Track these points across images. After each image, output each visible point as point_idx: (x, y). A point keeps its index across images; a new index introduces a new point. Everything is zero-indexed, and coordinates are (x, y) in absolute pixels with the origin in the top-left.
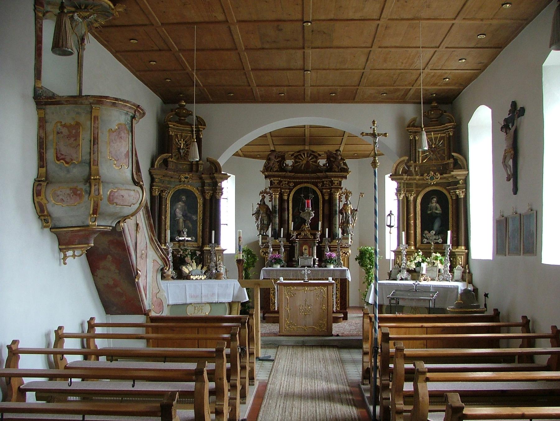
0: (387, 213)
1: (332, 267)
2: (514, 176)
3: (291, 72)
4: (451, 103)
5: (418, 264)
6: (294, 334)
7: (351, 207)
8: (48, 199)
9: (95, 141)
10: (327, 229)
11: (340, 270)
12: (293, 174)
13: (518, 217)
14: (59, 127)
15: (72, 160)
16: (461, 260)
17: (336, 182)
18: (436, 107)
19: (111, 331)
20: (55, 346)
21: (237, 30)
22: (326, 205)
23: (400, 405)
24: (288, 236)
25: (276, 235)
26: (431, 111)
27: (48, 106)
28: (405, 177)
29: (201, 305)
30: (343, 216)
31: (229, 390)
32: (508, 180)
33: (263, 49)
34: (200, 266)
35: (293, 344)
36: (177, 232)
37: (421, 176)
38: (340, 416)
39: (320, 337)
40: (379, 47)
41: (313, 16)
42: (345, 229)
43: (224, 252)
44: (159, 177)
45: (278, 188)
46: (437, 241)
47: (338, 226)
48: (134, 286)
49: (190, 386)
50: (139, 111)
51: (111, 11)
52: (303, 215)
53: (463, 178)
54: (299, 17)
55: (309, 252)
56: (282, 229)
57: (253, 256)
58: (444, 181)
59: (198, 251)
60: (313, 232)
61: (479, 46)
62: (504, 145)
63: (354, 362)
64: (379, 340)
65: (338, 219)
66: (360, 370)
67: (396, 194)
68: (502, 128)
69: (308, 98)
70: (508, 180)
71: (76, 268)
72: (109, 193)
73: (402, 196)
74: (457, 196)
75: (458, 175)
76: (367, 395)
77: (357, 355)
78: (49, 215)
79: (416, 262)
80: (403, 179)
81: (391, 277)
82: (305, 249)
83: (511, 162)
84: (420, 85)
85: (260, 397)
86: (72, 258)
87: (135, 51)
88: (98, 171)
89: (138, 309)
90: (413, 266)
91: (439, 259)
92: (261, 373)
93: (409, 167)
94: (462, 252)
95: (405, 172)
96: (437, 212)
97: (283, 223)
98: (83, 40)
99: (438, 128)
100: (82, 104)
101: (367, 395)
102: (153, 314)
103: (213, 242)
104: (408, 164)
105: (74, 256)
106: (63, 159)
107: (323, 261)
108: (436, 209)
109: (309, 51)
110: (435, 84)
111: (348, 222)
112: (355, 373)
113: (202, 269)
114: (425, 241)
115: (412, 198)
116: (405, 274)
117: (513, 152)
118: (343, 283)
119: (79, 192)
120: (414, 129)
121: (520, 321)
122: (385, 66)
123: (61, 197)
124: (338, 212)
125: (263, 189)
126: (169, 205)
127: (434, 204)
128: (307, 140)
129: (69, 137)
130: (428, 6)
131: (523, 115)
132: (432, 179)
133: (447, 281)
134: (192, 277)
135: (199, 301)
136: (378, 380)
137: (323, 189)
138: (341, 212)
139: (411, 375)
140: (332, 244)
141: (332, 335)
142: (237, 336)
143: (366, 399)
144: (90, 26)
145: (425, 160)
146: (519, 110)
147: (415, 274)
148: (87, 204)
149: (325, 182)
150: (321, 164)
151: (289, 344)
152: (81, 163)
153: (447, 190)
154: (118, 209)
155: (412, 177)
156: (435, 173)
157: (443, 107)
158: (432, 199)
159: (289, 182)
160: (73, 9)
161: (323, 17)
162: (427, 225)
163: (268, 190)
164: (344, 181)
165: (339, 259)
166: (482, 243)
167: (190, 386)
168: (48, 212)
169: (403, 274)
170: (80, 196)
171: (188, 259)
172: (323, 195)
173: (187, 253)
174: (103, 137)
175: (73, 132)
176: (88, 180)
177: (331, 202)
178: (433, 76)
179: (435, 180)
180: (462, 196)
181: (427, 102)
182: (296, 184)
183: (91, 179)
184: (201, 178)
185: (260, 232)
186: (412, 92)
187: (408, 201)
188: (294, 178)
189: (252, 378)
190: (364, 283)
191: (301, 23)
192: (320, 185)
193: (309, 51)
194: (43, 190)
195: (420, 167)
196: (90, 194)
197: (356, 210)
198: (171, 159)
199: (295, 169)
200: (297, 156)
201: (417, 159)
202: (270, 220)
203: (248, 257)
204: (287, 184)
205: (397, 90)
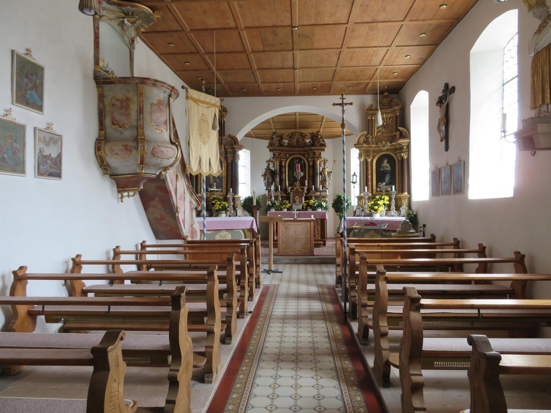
0: (352, 173)
2: (446, 138)
3: (285, 70)
4: (398, 93)
7: (327, 170)
8: (106, 152)
9: (141, 111)
13: (449, 168)
14: (114, 101)
15: (124, 125)
16: (405, 202)
18: (387, 96)
19: (159, 249)
20: (114, 259)
21: (244, 34)
23: (365, 300)
25: (276, 190)
26: (384, 98)
27: (105, 85)
31: (238, 291)
32: (442, 141)
33: (264, 51)
39: (307, 257)
40: (347, 48)
41: (299, 22)
48: (175, 219)
49: (202, 287)
50: (174, 92)
51: (151, 17)
53: (407, 144)
54: (288, 23)
58: (392, 147)
60: (302, 187)
61: (420, 44)
63: (330, 273)
64: (348, 253)
65: (319, 178)
66: (334, 277)
67: (359, 158)
68: (437, 103)
69: (297, 91)
70: (442, 141)
71: (132, 204)
72: (151, 149)
74: (402, 158)
75: (403, 143)
76: (340, 295)
77: (332, 268)
78: (108, 165)
80: (363, 147)
81: (355, 214)
83: (443, 128)
84: (376, 79)
85: (263, 296)
86: (127, 198)
87: (174, 54)
89: (178, 235)
92: (266, 280)
93: (367, 139)
95: (365, 142)
98: (133, 41)
99: (389, 110)
100: (130, 83)
101: (340, 295)
102: (189, 239)
105: (129, 196)
106: (118, 124)
108: (387, 167)
109: (297, 53)
110: (387, 78)
111: (325, 180)
112: (331, 280)
115: (369, 160)
117: (445, 120)
119: (129, 148)
120: (371, 112)
121: (452, 242)
122: (351, 64)
123: (116, 151)
125: (269, 159)
129: (121, 108)
130: (384, 10)
131: (453, 92)
132: (384, 146)
136: (347, 284)
138: (321, 174)
139: (372, 279)
141: (314, 255)
142: (246, 251)
143: (339, 298)
144: (137, 29)
146: (451, 89)
153: (395, 154)
154: (159, 161)
157: (392, 96)
159: (286, 154)
160: (123, 15)
161: (306, 23)
162: (380, 179)
163: (272, 159)
166: (421, 188)
167: (202, 287)
168: (107, 163)
170: (130, 151)
172: (308, 162)
174: (147, 109)
175: (125, 104)
176: (136, 140)
177: (314, 167)
178: (386, 71)
180: (406, 157)
181: (382, 93)
182: (290, 155)
183: (139, 139)
186: (370, 85)
189: (258, 283)
191: (290, 28)
192: (307, 155)
193: (297, 53)
194: (103, 146)
195: (376, 138)
196: (137, 149)
199: (289, 145)
202: (274, 180)
205: (359, 84)
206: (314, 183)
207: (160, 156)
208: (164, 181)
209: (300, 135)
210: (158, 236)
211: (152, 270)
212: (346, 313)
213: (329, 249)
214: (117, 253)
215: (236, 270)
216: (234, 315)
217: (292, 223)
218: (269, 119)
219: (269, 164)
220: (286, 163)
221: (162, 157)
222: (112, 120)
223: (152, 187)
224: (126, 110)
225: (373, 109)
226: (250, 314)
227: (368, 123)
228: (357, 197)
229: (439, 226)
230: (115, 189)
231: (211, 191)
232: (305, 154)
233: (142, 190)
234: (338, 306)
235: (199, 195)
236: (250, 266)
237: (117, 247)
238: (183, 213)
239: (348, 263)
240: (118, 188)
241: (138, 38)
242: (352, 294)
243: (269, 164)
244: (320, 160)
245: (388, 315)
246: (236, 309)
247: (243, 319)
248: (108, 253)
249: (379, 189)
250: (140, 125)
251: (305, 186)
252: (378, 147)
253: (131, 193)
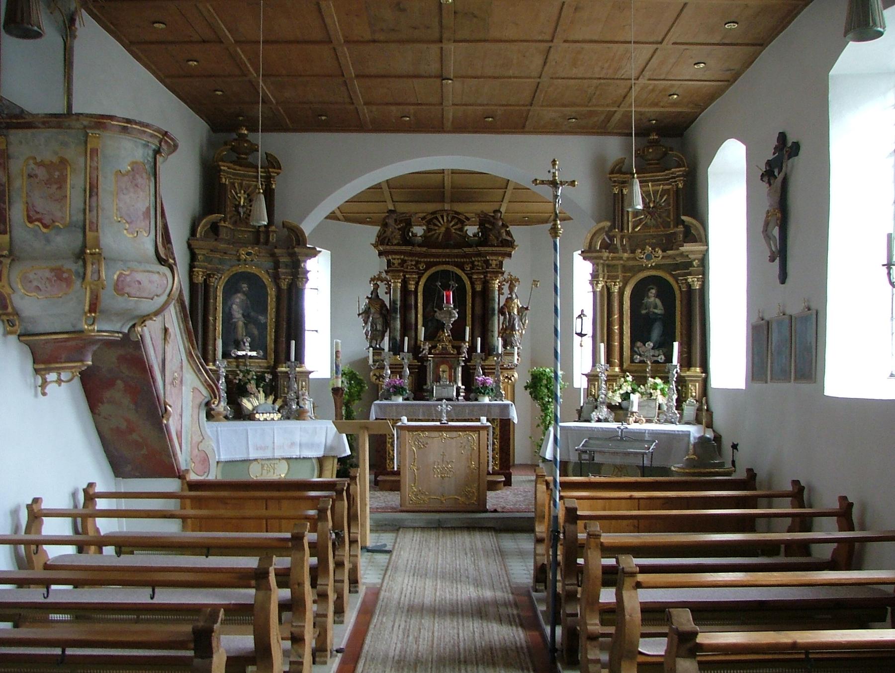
0: (577, 312)
1: (486, 400)
2: (781, 254)
3: (420, 80)
5: (626, 396)
6: (425, 509)
7: (518, 303)
9: (92, 190)
10: (479, 339)
11: (500, 405)
12: (424, 249)
14: (33, 166)
16: (694, 389)
20: (28, 530)
22: (478, 301)
23: (594, 625)
24: (415, 349)
25: (396, 348)
27: (12, 131)
29: (273, 462)
30: (505, 318)
31: (315, 602)
32: (772, 260)
33: (374, 41)
34: (271, 398)
39: (465, 513)
40: (565, 41)
43: (311, 376)
46: (656, 358)
47: (496, 334)
48: (161, 430)
50: (166, 142)
52: (439, 315)
55: (450, 376)
56: (406, 338)
57: (359, 383)
59: (268, 373)
62: (766, 203)
63: (521, 554)
64: (561, 519)
65: (497, 323)
67: (591, 283)
68: (762, 176)
69: (448, 125)
70: (772, 260)
71: (63, 400)
72: (115, 277)
73: (600, 286)
74: (689, 286)
75: (692, 252)
76: (541, 608)
77: (526, 543)
79: (622, 392)
80: (601, 258)
82: (444, 371)
83: (776, 232)
86: (56, 385)
89: (162, 464)
90: (617, 399)
91: (659, 387)
92: (368, 576)
93: (612, 238)
95: (605, 246)
96: (656, 311)
97: (407, 328)
98: (72, 21)
99: (660, 175)
100: (69, 127)
101: (541, 608)
102: (193, 477)
105: (59, 381)
106: (40, 220)
107: (472, 390)
108: (656, 307)
109: (450, 47)
110: (656, 104)
111: (512, 328)
112: (522, 572)
114: (638, 358)
115: (616, 289)
116: (604, 412)
117: (779, 215)
118: (504, 427)
119: (65, 275)
120: (621, 177)
121: (789, 488)
122: (574, 72)
123: (35, 283)
124: (496, 312)
125: (376, 274)
127: (652, 299)
128: (448, 194)
129: (48, 183)
131: (797, 154)
132: (649, 257)
133: (672, 423)
134: (257, 416)
135: (269, 455)
136: (559, 585)
137: (472, 274)
138: (502, 312)
140: (487, 363)
141: (486, 511)
142: (329, 513)
143: (541, 617)
150: (470, 234)
152: (70, 226)
154: (131, 303)
158: (649, 290)
159: (418, 262)
162: (640, 334)
163: (384, 275)
164: (506, 262)
165: (498, 386)
166: (728, 362)
168: (13, 308)
170: (68, 282)
171: (252, 387)
173: (249, 377)
174: (107, 184)
176: (81, 256)
177: (485, 295)
178: (653, 90)
179: (652, 260)
181: (642, 133)
182: (429, 266)
184: (273, 255)
185: (371, 343)
186: (617, 116)
187: (610, 294)
188: (425, 255)
189: (354, 581)
192: (468, 268)
195: (630, 238)
196: (84, 278)
197: (527, 309)
199: (427, 241)
200: (430, 221)
201: (625, 226)
202: (387, 324)
203: (350, 384)
204: (415, 265)
205: (591, 114)
206: (485, 334)
207: (133, 291)
208: (139, 345)
209: (453, 218)
212: (553, 650)
215: (312, 555)
216: (307, 658)
217: (436, 434)
218: (380, 184)
219: (376, 287)
220: (417, 284)
221: (138, 294)
222: (27, 211)
223: (111, 357)
224: (60, 188)
225: (623, 170)
226: (340, 655)
228: (586, 375)
229: (773, 449)
230: (29, 365)
231: (238, 357)
232: (464, 263)
233: (89, 367)
234: (536, 633)
235: (211, 367)
236: (338, 543)
237: (36, 500)
238: (177, 417)
239: (561, 536)
240: (35, 362)
241: (83, 10)
242: (569, 610)
243: (376, 287)
244: (501, 278)
245: (641, 659)
246: (310, 641)
247: (324, 666)
248: (15, 513)
249: (638, 358)
250: (91, 223)
251: (464, 340)
252: (634, 259)
253: (64, 376)
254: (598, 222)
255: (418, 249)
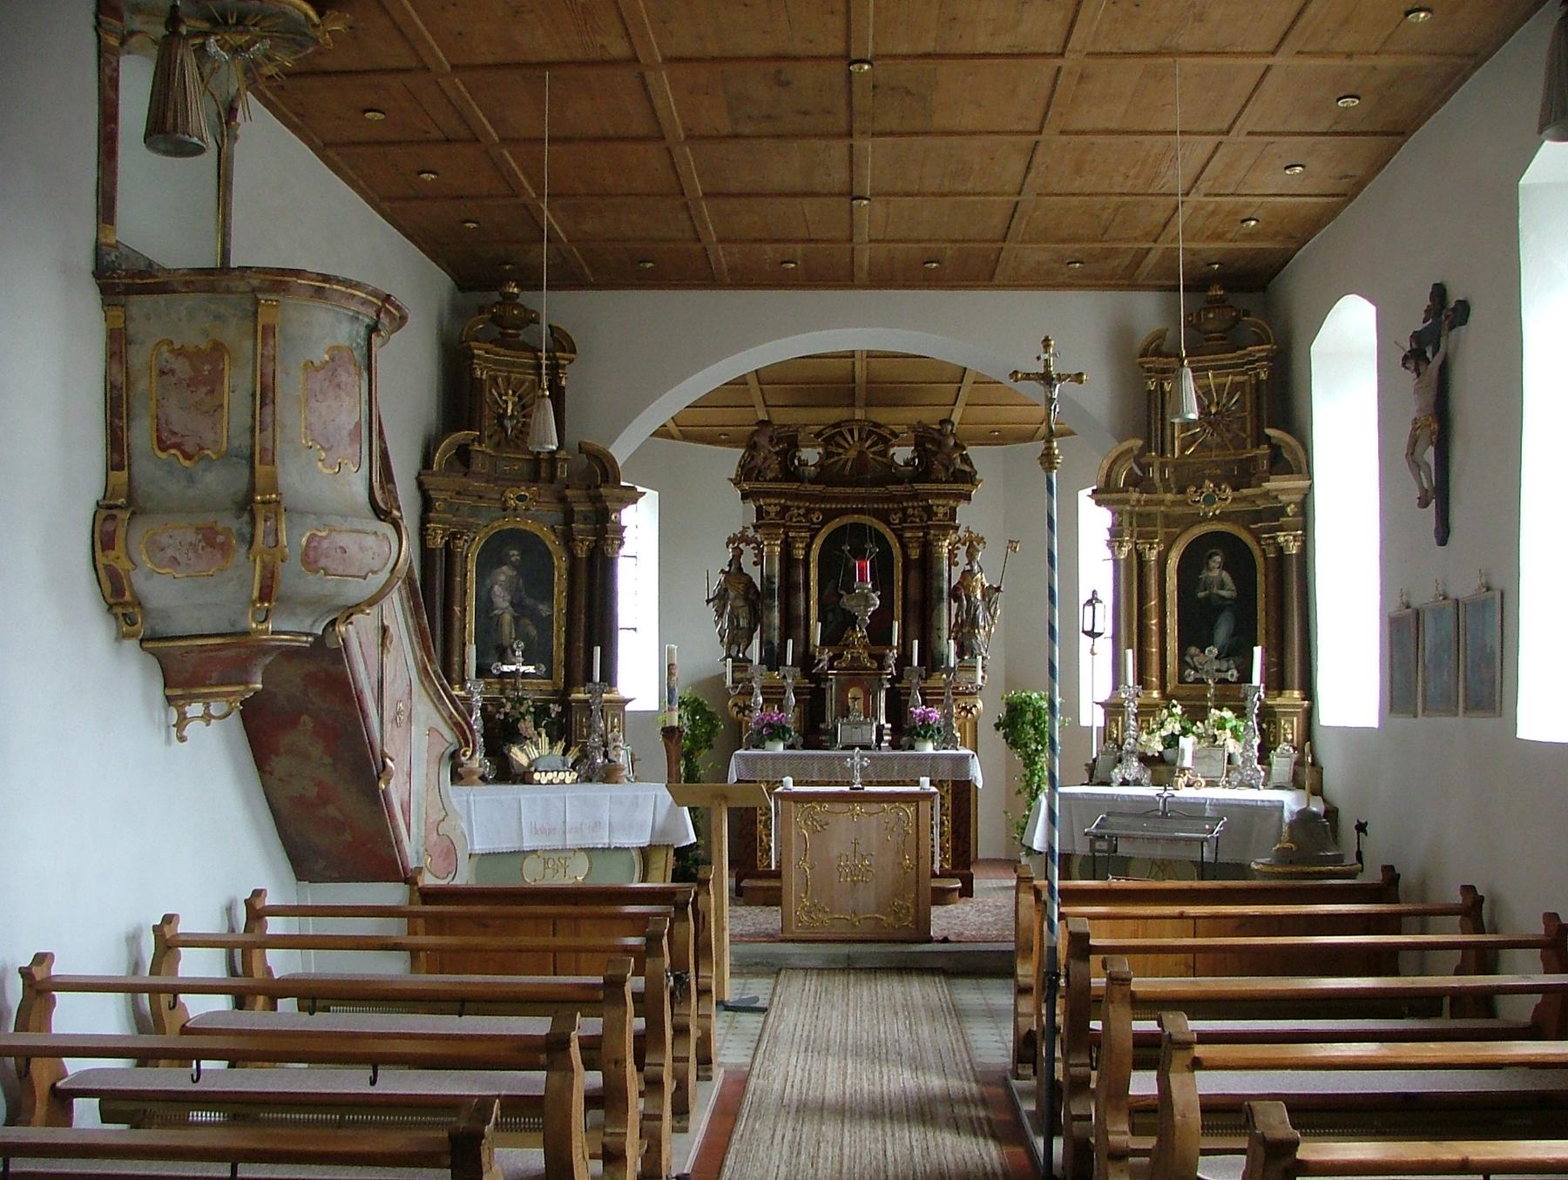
0: (1084, 596)
1: (929, 748)
2: (1439, 494)
3: (816, 200)
4: (1264, 289)
5: (1172, 741)
6: (824, 936)
7: (982, 580)
8: (136, 557)
9: (265, 395)
10: (916, 642)
11: (952, 757)
12: (819, 488)
13: (1450, 609)
14: (166, 355)
15: (202, 449)
16: (1290, 729)
17: (941, 510)
18: (1221, 300)
19: (311, 926)
20: (155, 970)
21: (663, 83)
22: (914, 575)
24: (806, 661)
25: (772, 659)
26: (1208, 310)
27: (134, 298)
28: (1134, 496)
29: (564, 855)
30: (960, 606)
31: (641, 1094)
32: (1424, 503)
33: (737, 136)
34: (561, 745)
35: (819, 963)
36: (495, 649)
37: (1179, 492)
38: (952, 1167)
39: (896, 946)
40: (1062, 132)
41: (876, 44)
42: (966, 643)
43: (628, 707)
44: (446, 495)
45: (778, 526)
46: (1222, 675)
47: (945, 633)
48: (376, 801)
49: (532, 1081)
50: (388, 312)
52: (847, 602)
53: (1297, 498)
54: (838, 47)
55: (866, 706)
56: (790, 642)
57: (710, 718)
58: (1243, 507)
59: (555, 702)
60: (876, 650)
61: (1341, 128)
62: (1412, 407)
63: (992, 1014)
64: (1062, 954)
65: (947, 614)
66: (1009, 1036)
67: (1110, 544)
68: (1405, 359)
69: (862, 275)
70: (1424, 503)
71: (212, 750)
72: (304, 540)
73: (1125, 549)
74: (1280, 550)
75: (1283, 491)
76: (1028, 1106)
77: (1000, 996)
78: (138, 602)
79: (1164, 733)
80: (1127, 502)
81: (1095, 775)
82: (855, 699)
83: (1430, 455)
84: (1176, 239)
85: (728, 1113)
86: (202, 723)
87: (378, 143)
88: (274, 478)
89: (387, 866)
90: (1157, 746)
91: (1228, 725)
92: (731, 1046)
94: (1294, 706)
95: (1134, 482)
96: (1223, 593)
97: (792, 624)
98: (231, 111)
99: (1227, 358)
100: (228, 291)
101: (1028, 1106)
102: (428, 880)
103: (597, 678)
104: (1143, 460)
105: (207, 717)
106: (177, 446)
107: (904, 731)
108: (1222, 586)
109: (865, 144)
110: (1219, 236)
111: (974, 623)
112: (994, 1045)
113: (564, 754)
114: (1191, 674)
115: (1152, 556)
116: (1133, 768)
117: (1435, 426)
118: (961, 794)
119: (220, 539)
120: (1160, 362)
121: (1457, 899)
122: (1077, 184)
123: (170, 552)
124: (945, 595)
125: (737, 530)
126: (472, 576)
127: (1216, 573)
128: (860, 393)
129: (193, 383)
130: (1200, 18)
131: (1464, 322)
132: (1209, 500)
133: (1252, 787)
134: (537, 776)
135: (556, 843)
136: (1059, 1066)
137: (903, 529)
138: (954, 594)
139: (1151, 1052)
140: (930, 683)
141: (930, 940)
142: (665, 941)
143: (1026, 1120)
144: (251, 73)
145: (1189, 447)
146: (1454, 310)
147: (1161, 768)
148: (244, 573)
149: (910, 511)
150: (899, 460)
151: (809, 964)
152: (226, 456)
153: (1251, 531)
155: (1154, 497)
156: (1217, 485)
157: (1242, 300)
158: (1210, 556)
159: (809, 511)
160: (205, 26)
161: (904, 49)
162: (1195, 631)
163: (751, 533)
164: (962, 509)
165: (949, 725)
166: (1349, 680)
167: (532, 1081)
168: (134, 594)
169: (1127, 767)
170: (225, 549)
171: (526, 726)
172: (904, 546)
173: (523, 709)
174: (289, 384)
175: (204, 369)
176: (245, 505)
177: (926, 566)
178: (1213, 213)
179: (1218, 504)
180: (1293, 549)
181: (1197, 285)
182: (829, 516)
183: (254, 503)
184: (562, 499)
185: (728, 649)
186: (1152, 258)
187: (1142, 563)
188: (823, 499)
189: (705, 1061)
190: (1019, 792)
191: (844, 64)
192: (895, 519)
193: (865, 144)
194: (120, 533)
195: (1177, 467)
196: (251, 543)
197: (998, 589)
198: (480, 444)
199: (825, 474)
200: (830, 438)
201: (1168, 447)
202: (756, 618)
203: (694, 720)
205: (1110, 253)
210: (304, 864)
211: (287, 1005)
213: (981, 912)
214: (168, 941)
227: (1148, 412)
233: (256, 692)
237: (169, 919)
248: (133, 939)
254: (1120, 442)
255: (810, 487)
